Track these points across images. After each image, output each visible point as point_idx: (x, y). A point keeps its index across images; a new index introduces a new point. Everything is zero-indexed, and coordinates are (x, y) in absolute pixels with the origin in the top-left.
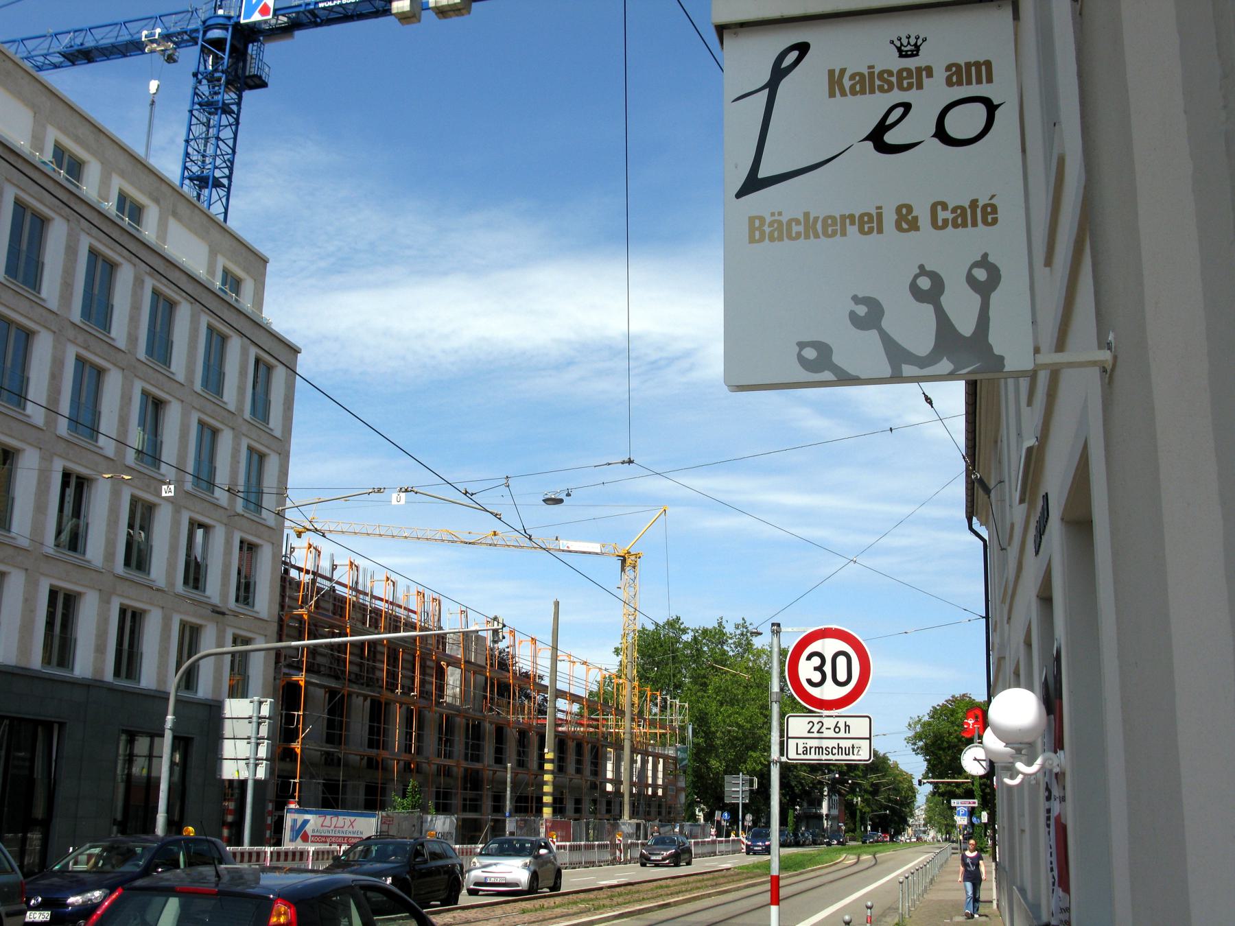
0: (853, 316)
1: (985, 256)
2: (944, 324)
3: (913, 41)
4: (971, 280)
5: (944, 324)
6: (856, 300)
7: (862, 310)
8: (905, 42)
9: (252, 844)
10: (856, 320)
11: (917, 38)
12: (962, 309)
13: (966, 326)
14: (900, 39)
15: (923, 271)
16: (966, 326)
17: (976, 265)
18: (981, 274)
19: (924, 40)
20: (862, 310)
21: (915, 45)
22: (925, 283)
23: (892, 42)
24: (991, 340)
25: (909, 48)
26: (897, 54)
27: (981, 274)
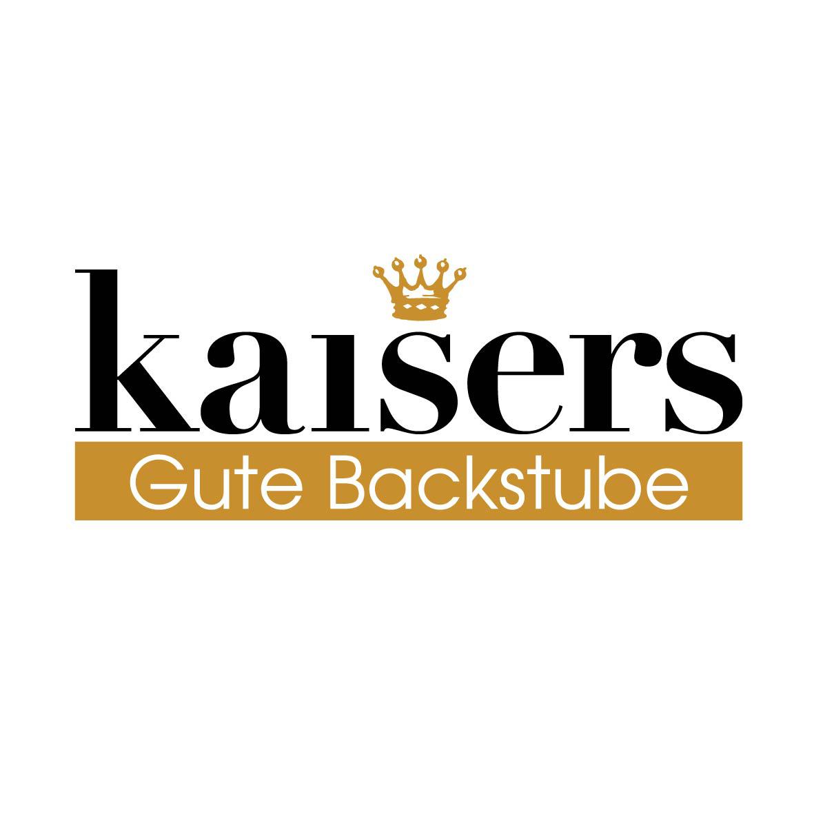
0: (416, 260)
1: (465, 268)
2: (440, 280)
3: (431, 276)
4: (456, 273)
5: (440, 280)
6: (421, 256)
7: (420, 260)
8: (411, 275)
9: (338, 486)
10: (416, 262)
11: (443, 267)
12: (448, 279)
13: (445, 285)
14: (398, 266)
15: (445, 261)
16: (445, 285)
17: (460, 269)
18: (460, 273)
19: (461, 275)
20: (420, 260)
21: (437, 286)
22: (443, 265)
23: (379, 272)
24: (450, 294)
25: (420, 293)
26: (391, 308)
27: (460, 273)
